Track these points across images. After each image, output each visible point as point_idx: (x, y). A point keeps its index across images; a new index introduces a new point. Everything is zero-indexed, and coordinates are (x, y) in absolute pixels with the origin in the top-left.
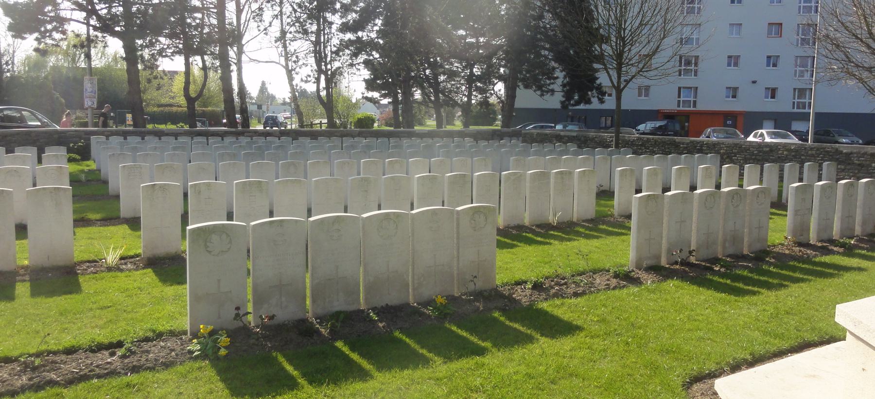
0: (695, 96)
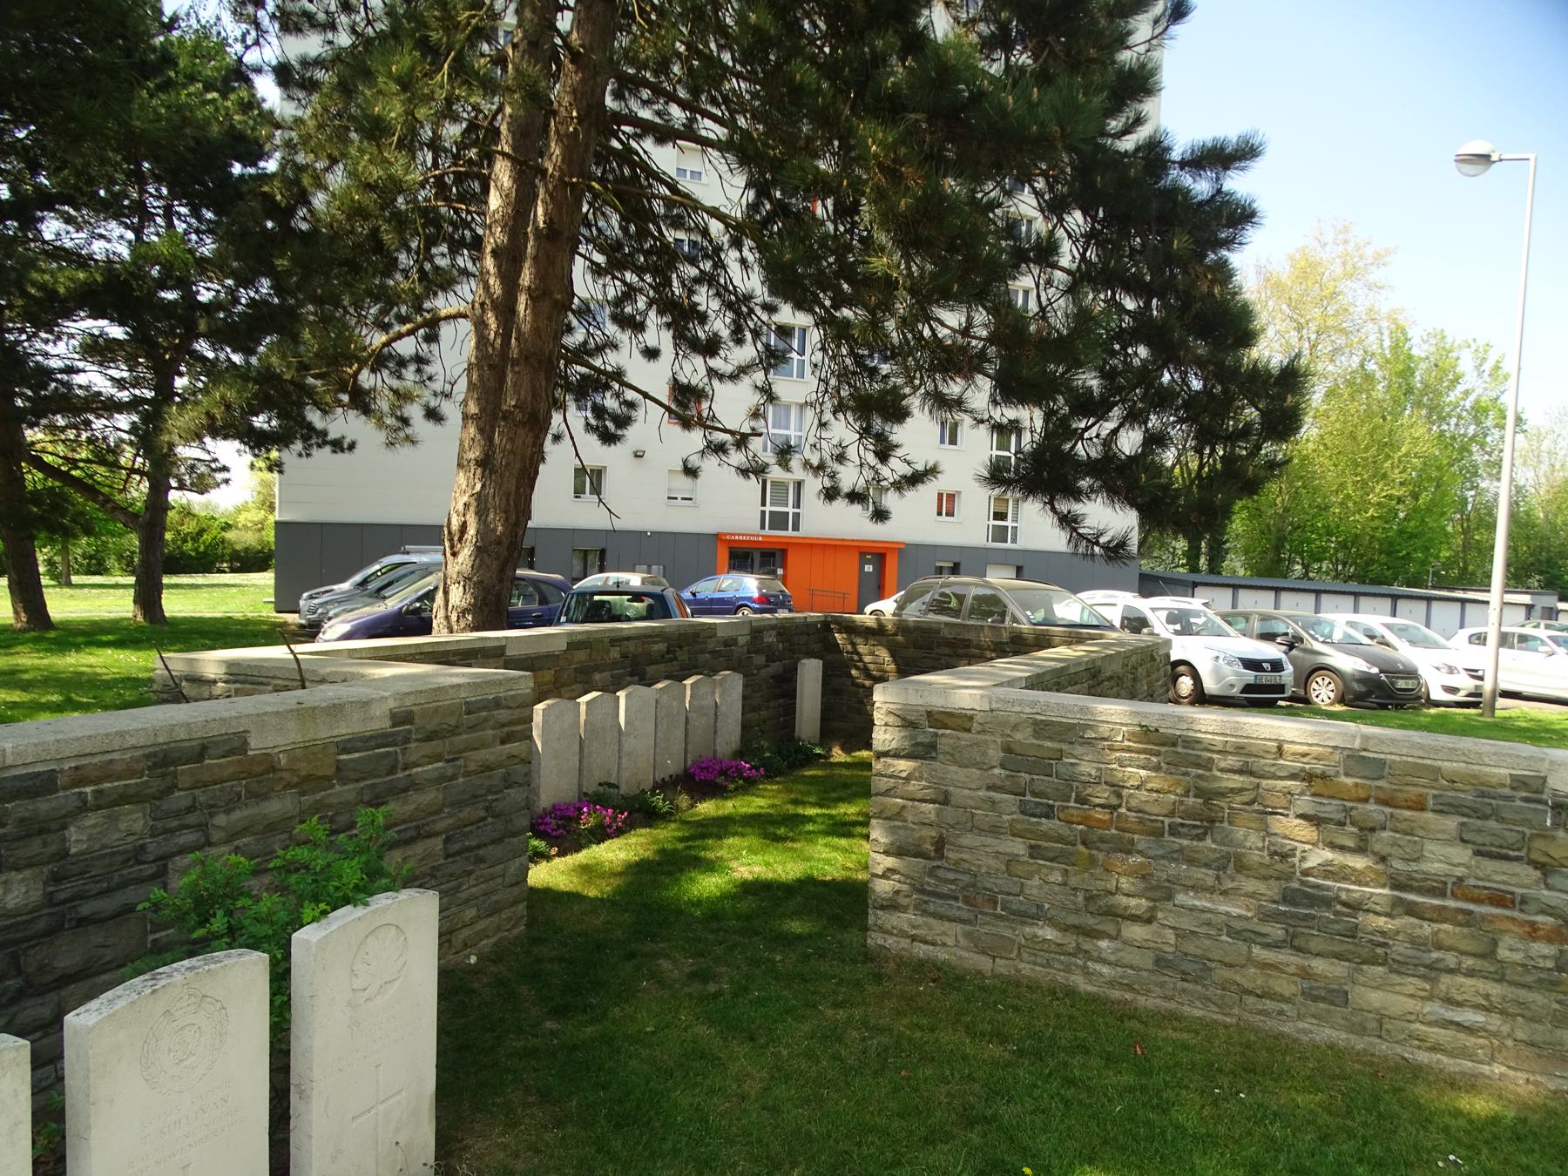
0: (797, 505)
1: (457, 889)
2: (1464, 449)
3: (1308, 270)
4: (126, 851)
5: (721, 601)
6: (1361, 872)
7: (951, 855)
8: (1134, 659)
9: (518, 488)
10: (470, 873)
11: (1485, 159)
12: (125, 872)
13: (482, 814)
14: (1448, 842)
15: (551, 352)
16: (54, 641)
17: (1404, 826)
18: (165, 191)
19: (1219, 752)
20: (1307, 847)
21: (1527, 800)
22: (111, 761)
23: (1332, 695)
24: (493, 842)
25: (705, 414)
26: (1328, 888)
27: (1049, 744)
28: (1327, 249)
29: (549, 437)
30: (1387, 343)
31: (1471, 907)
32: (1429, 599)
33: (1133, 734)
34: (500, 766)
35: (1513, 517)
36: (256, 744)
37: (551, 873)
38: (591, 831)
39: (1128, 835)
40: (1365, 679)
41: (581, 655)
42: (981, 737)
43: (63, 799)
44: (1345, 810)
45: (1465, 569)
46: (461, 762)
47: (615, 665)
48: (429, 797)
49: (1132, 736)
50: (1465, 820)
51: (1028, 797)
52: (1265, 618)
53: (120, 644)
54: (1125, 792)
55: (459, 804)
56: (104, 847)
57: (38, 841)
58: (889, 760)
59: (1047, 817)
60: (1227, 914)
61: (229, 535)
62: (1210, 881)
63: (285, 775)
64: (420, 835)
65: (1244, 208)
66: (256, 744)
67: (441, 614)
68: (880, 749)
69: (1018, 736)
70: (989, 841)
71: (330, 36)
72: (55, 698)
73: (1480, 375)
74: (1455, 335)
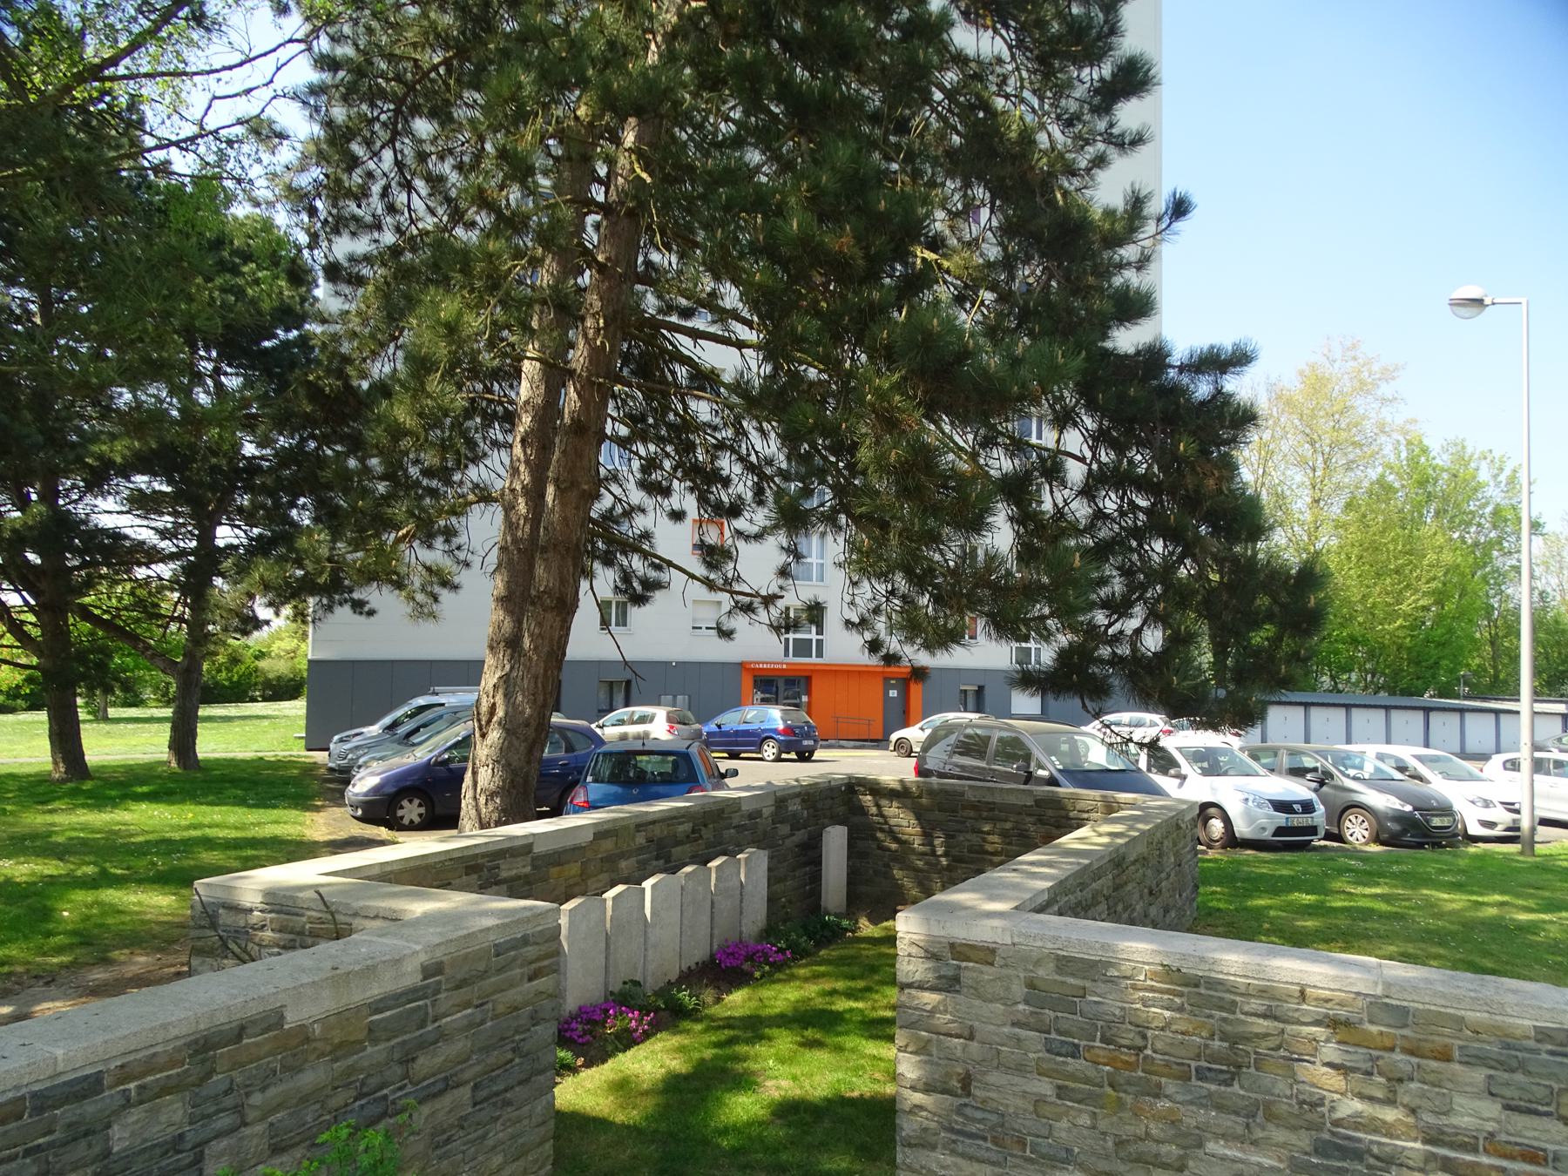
1: (484, 1137)
2: (1487, 554)
3: (1317, 384)
4: (166, 1142)
5: (746, 733)
6: (1391, 1125)
7: (977, 1093)
8: (1159, 835)
9: (546, 671)
10: (498, 1118)
11: (1479, 302)
12: (163, 1163)
13: (509, 1056)
14: (1477, 1096)
15: (579, 540)
16: (90, 794)
17: (1431, 1077)
18: (214, 354)
19: (1242, 995)
20: (1336, 1096)
21: (1552, 1053)
22: (154, 1055)
23: (1366, 834)
24: (520, 1083)
25: (730, 575)
26: (1359, 1140)
27: (1071, 980)
28: (1337, 365)
30: (1404, 455)
31: (1504, 1163)
32: (1462, 711)
33: (1155, 973)
34: (527, 1004)
35: (1537, 625)
36: (292, 1019)
37: (582, 1091)
38: (617, 1036)
39: (1155, 1078)
40: (1400, 817)
41: (608, 845)
42: (1005, 971)
43: (110, 1096)
44: (1373, 1059)
45: (1496, 676)
46: (490, 1006)
47: (640, 850)
48: (459, 1046)
49: (1154, 976)
50: (1492, 1072)
51: (1053, 1036)
52: (1293, 753)
53: (153, 797)
54: (1149, 1033)
55: (486, 1049)
56: (145, 1140)
57: (83, 1143)
58: (913, 992)
59: (1073, 1057)
60: (1259, 1164)
61: (262, 664)
62: (1240, 1130)
63: (319, 1045)
64: (448, 1085)
65: (1245, 411)
66: (292, 1019)
67: (470, 794)
68: (904, 980)
69: (1041, 972)
70: (1016, 1080)
71: (376, 235)
72: (90, 870)
73: (1498, 484)
74: (1474, 446)
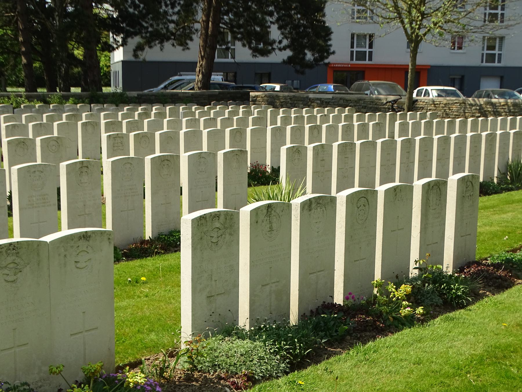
0: (371, 46)
29: (137, 60)
